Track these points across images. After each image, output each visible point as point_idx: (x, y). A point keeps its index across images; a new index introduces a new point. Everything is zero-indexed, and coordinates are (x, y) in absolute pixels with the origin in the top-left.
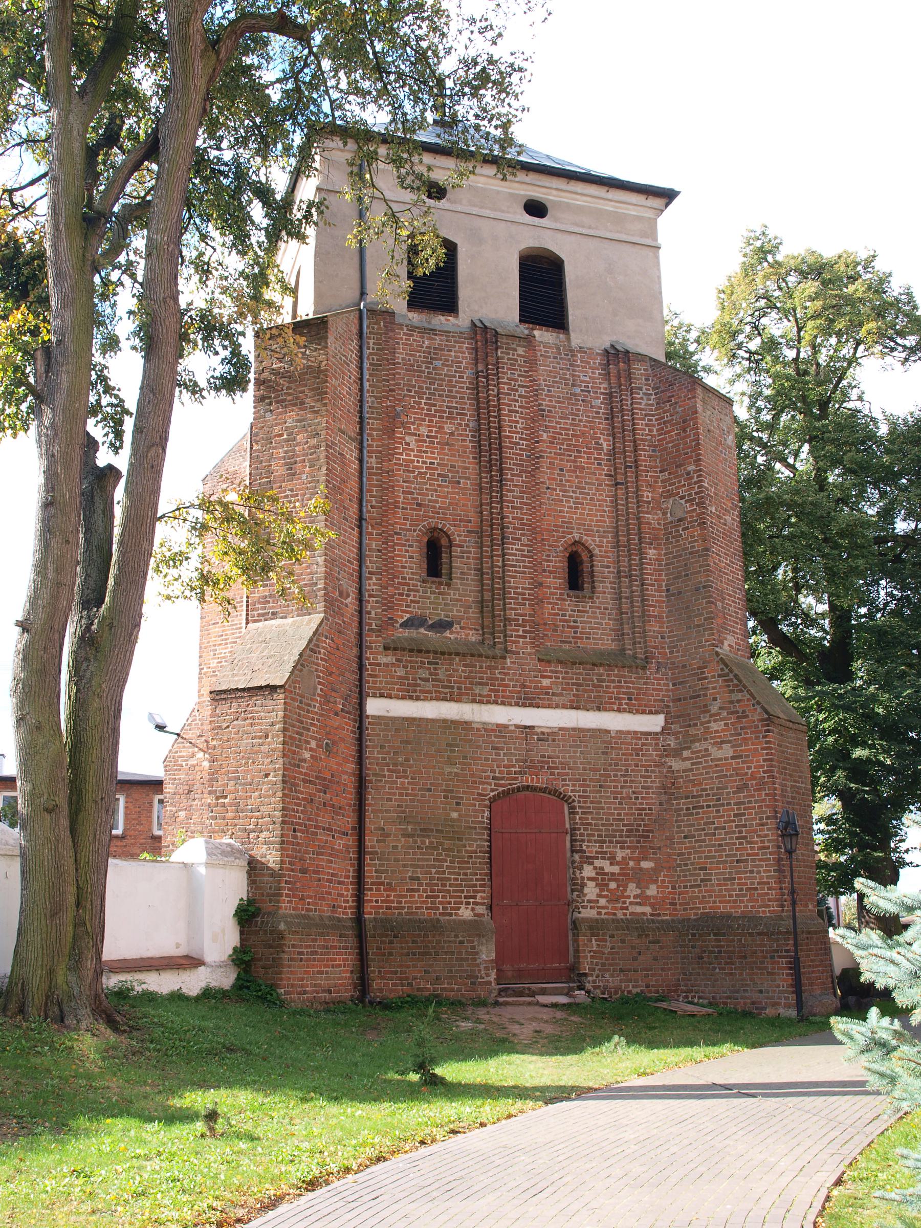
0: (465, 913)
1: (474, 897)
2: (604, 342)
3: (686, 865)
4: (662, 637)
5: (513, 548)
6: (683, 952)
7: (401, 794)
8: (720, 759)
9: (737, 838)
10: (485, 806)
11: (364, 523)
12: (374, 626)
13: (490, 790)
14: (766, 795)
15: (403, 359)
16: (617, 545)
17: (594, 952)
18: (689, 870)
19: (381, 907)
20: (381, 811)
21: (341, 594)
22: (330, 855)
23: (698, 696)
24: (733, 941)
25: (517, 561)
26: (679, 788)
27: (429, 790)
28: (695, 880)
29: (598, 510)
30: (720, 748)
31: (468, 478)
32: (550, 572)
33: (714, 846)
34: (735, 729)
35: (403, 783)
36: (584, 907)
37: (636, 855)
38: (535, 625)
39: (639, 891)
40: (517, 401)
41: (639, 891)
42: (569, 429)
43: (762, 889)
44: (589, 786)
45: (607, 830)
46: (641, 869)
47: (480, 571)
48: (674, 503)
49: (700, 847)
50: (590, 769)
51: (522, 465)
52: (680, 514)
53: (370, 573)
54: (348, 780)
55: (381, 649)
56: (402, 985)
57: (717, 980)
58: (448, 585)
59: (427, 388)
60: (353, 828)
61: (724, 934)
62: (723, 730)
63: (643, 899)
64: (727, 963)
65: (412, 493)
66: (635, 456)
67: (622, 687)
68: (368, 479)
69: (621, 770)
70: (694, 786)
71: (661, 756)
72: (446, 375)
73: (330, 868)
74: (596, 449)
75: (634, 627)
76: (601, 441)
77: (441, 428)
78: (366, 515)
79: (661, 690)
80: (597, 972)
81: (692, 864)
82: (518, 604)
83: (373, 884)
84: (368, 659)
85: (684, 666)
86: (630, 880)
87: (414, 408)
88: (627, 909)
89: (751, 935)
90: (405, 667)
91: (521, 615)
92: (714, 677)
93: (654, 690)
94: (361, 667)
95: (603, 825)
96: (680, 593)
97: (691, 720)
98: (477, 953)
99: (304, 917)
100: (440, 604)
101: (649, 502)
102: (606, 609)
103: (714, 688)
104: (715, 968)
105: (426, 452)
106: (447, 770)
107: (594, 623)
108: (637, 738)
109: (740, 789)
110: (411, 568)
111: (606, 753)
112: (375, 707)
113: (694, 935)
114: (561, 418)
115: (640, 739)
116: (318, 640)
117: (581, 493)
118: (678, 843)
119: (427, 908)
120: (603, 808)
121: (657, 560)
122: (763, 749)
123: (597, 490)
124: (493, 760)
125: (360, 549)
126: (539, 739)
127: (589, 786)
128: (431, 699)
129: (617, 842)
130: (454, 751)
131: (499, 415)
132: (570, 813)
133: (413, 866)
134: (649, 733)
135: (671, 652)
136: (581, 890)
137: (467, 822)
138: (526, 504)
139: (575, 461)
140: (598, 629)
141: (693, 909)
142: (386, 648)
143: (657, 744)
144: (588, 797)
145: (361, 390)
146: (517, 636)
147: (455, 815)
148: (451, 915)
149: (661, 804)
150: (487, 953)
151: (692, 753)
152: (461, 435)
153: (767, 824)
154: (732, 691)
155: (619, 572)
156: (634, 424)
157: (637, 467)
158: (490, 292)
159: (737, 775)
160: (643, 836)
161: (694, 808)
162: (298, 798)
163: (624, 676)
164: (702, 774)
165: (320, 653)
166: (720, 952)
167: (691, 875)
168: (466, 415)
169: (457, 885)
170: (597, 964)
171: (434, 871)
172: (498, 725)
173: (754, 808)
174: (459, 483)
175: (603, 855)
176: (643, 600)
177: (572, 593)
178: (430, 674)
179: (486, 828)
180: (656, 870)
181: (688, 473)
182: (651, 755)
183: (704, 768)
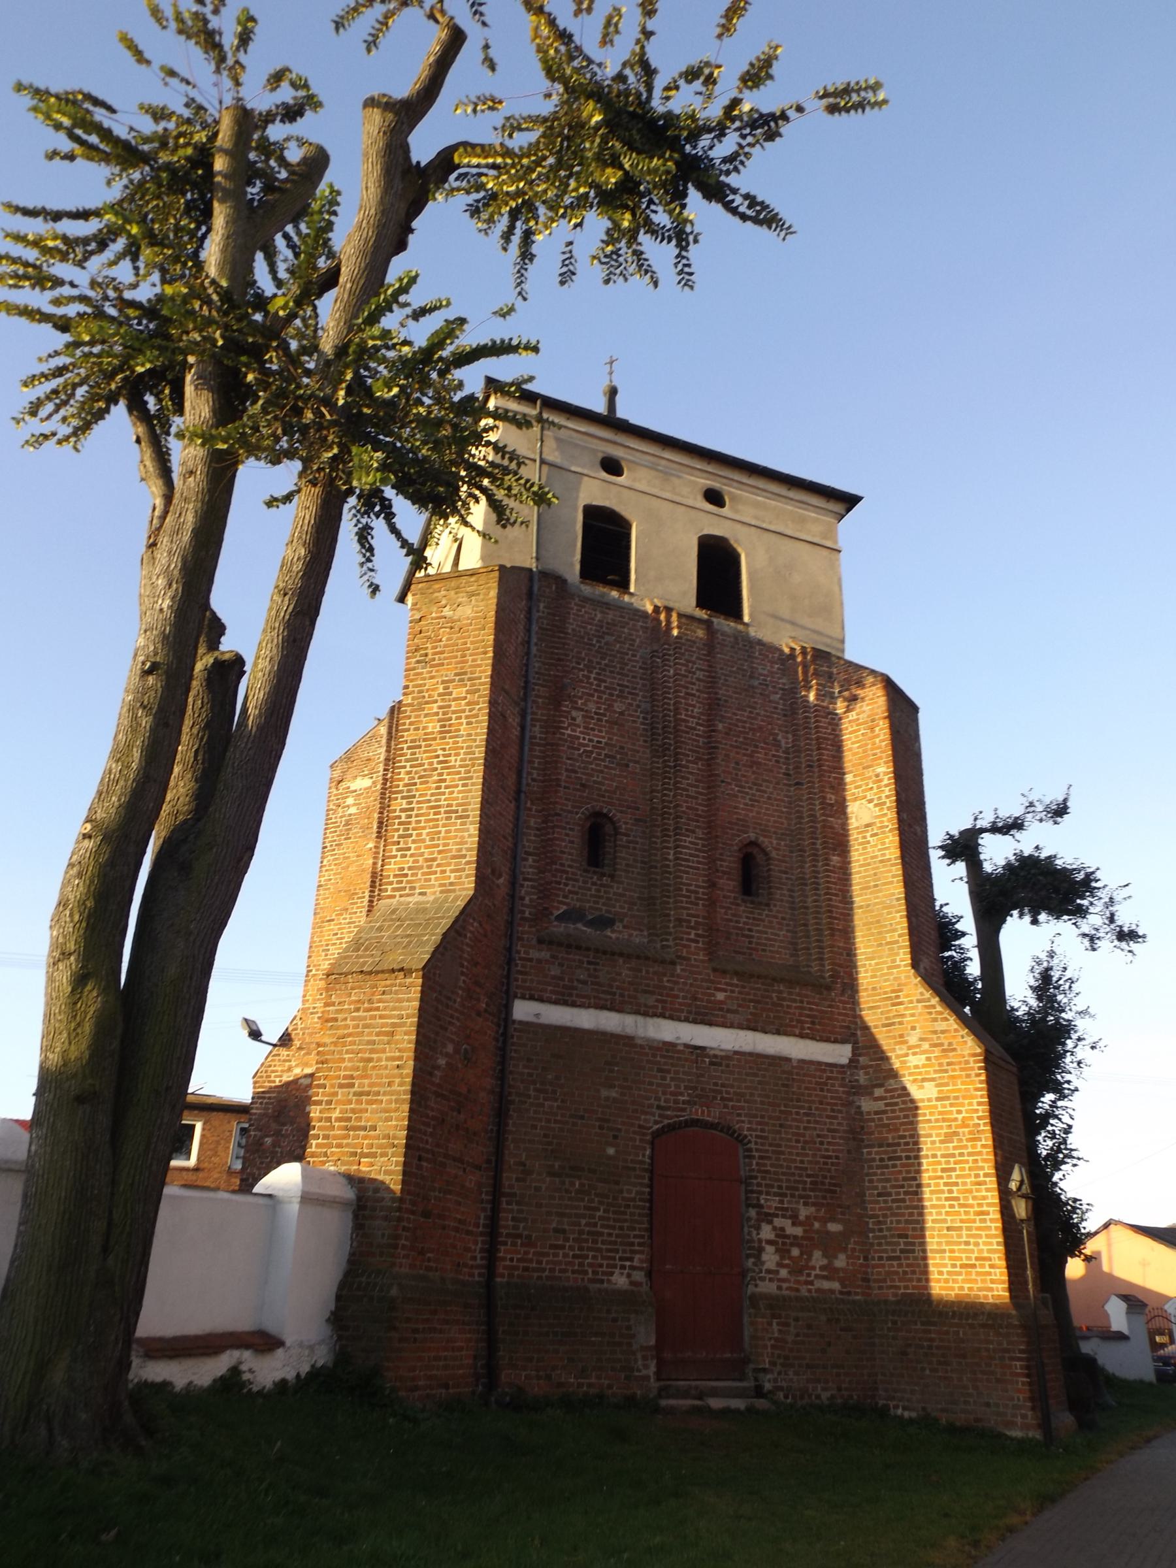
0: (620, 1281)
1: (631, 1259)
7: (548, 1121)
9: (947, 1199)
11: (523, 796)
12: (527, 915)
15: (573, 630)
17: (776, 1339)
18: (885, 1237)
19: (517, 1268)
21: (493, 872)
23: (893, 1024)
24: (947, 1333)
25: (691, 855)
27: (582, 1118)
28: (894, 1251)
29: (776, 811)
30: (922, 1087)
32: (724, 873)
34: (940, 1065)
36: (762, 1279)
37: (822, 1213)
39: (825, 1262)
40: (694, 684)
41: (825, 1262)
42: (745, 722)
43: (983, 1266)
44: (767, 1124)
45: (788, 1181)
46: (828, 1232)
49: (899, 1208)
51: (698, 752)
52: (867, 819)
53: (527, 853)
55: (534, 942)
58: (612, 876)
60: (489, 1161)
61: (934, 1324)
62: (924, 1066)
63: (830, 1272)
65: (576, 772)
68: (531, 750)
69: (802, 1107)
70: (890, 1131)
71: (848, 1093)
72: (618, 652)
74: (774, 745)
76: (779, 738)
77: (611, 706)
78: (524, 788)
80: (779, 1368)
81: (889, 1229)
82: (691, 903)
83: (508, 1235)
85: (874, 989)
87: (582, 681)
88: (811, 1283)
89: (972, 1326)
90: (561, 965)
91: (694, 916)
92: (911, 1002)
93: (840, 1014)
94: (510, 961)
95: (783, 1174)
98: (634, 1336)
100: (601, 897)
101: (831, 805)
102: (783, 919)
103: (912, 1015)
104: (923, 1369)
105: (593, 729)
106: (604, 1093)
109: (948, 1138)
110: (570, 854)
113: (894, 1323)
116: (464, 921)
117: (758, 790)
119: (573, 1272)
120: (783, 1153)
123: (775, 788)
124: (659, 1085)
125: (516, 826)
126: (712, 1063)
127: (767, 1124)
128: (589, 1007)
129: (801, 1197)
130: (612, 1071)
138: (701, 794)
139: (752, 756)
140: (775, 940)
142: (540, 941)
143: (843, 1079)
144: (766, 1138)
145: (528, 654)
146: (688, 940)
147: (611, 1151)
148: (602, 1281)
149: (849, 1152)
151: (887, 1091)
152: (632, 716)
153: (985, 1183)
154: (935, 1020)
159: (944, 1120)
161: (890, 1159)
162: (427, 1116)
163: (807, 996)
164: (898, 1118)
165: (465, 936)
166: (930, 1347)
167: (888, 1244)
169: (610, 1243)
170: (779, 1357)
171: (583, 1222)
172: (665, 1043)
173: (967, 1162)
174: (627, 766)
175: (783, 1212)
177: (746, 898)
178: (589, 976)
179: (645, 1170)
181: (877, 776)
182: (837, 1092)
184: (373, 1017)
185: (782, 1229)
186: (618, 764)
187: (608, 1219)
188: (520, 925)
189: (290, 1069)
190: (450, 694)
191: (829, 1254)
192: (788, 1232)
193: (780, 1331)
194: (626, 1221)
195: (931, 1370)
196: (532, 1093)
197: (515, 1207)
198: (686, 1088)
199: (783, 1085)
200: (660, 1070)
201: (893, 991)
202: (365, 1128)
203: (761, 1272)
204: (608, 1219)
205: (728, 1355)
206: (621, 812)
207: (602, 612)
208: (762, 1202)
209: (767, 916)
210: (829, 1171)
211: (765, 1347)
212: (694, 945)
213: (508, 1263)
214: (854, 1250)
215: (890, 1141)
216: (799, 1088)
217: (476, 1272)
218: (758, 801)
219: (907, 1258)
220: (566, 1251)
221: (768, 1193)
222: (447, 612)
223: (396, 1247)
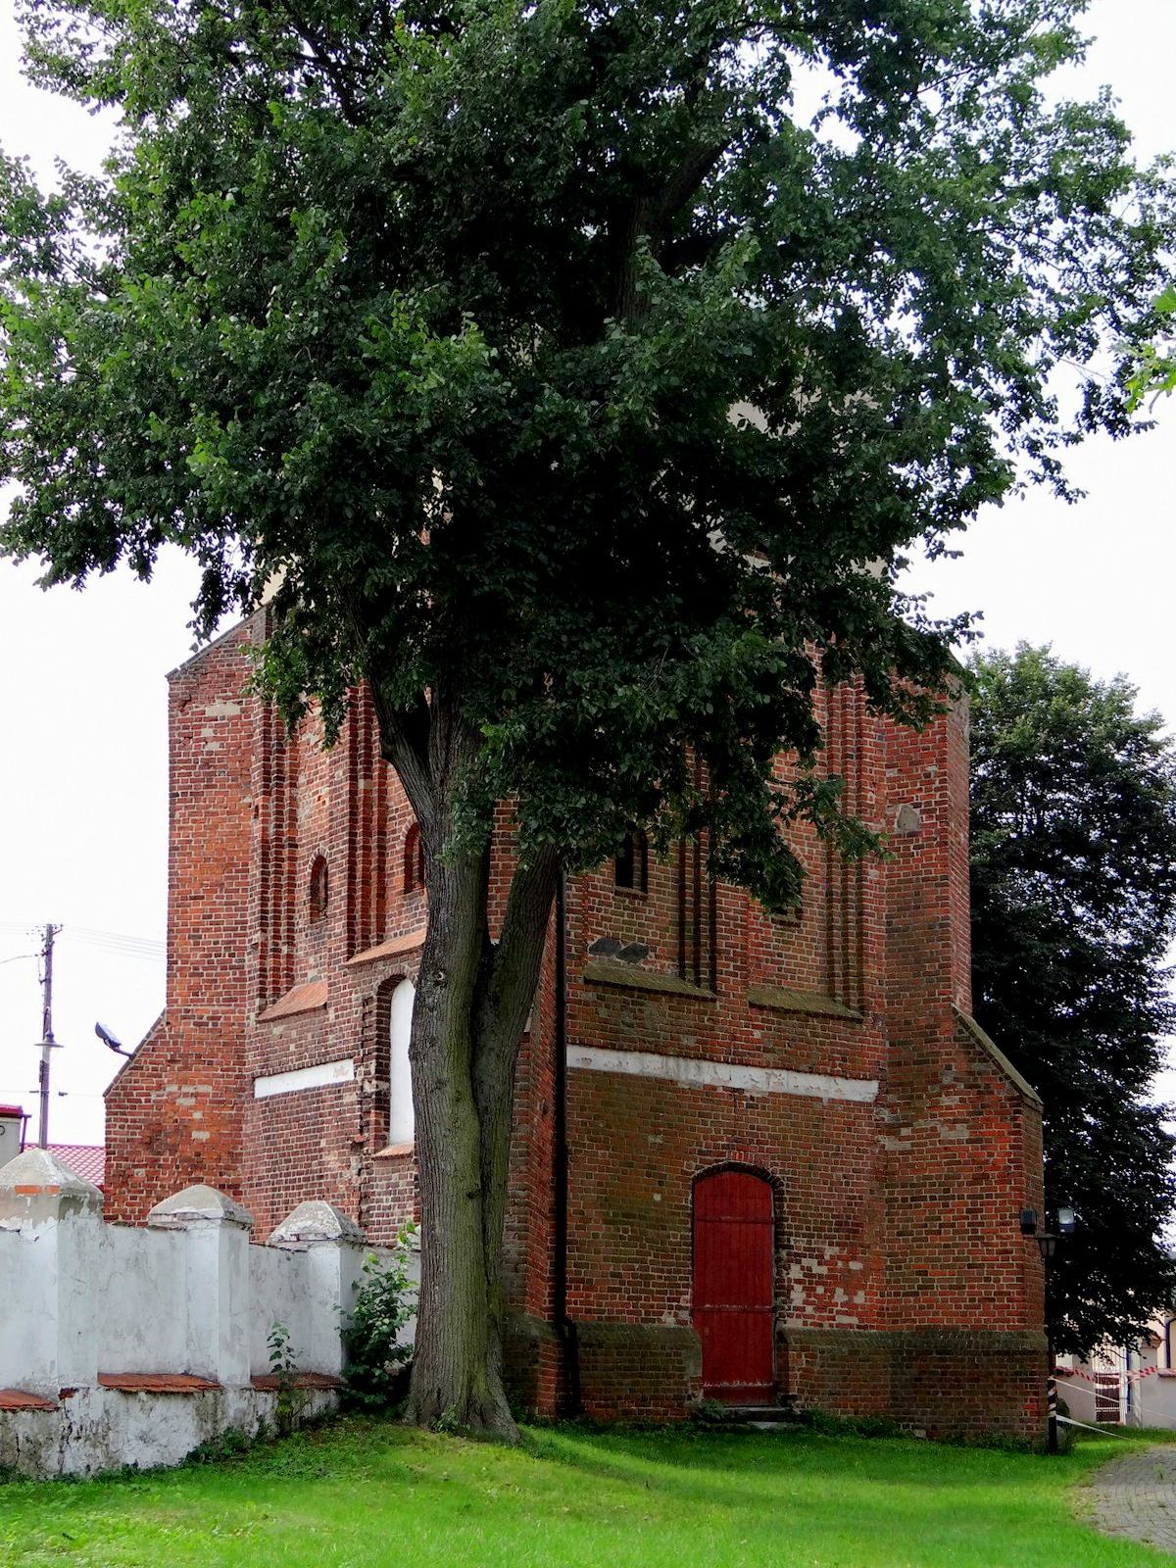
0: (669, 1320)
6: (895, 1373)
8: (952, 1142)
14: (1012, 1189)
30: (951, 1129)
39: (846, 1298)
41: (846, 1298)
46: (849, 1271)
52: (912, 826)
55: (581, 981)
56: (606, 1406)
58: (644, 899)
63: (850, 1308)
75: (848, 967)
79: (876, 1050)
82: (730, 931)
86: (837, 1284)
93: (870, 1049)
95: (812, 1215)
97: (913, 1090)
106: (651, 1139)
109: (976, 1180)
112: (575, 1056)
118: (889, 1241)
120: (812, 1195)
121: (878, 883)
129: (826, 1237)
133: (614, 1260)
137: (670, 1207)
141: (905, 1321)
146: (727, 973)
147: (657, 1197)
148: (653, 1321)
149: (872, 1192)
150: (694, 1369)
161: (913, 1199)
169: (660, 1285)
171: (637, 1266)
172: (705, 1086)
180: (864, 1273)
181: (928, 775)
189: (160, 1087)
191: (850, 1292)
214: (872, 1287)
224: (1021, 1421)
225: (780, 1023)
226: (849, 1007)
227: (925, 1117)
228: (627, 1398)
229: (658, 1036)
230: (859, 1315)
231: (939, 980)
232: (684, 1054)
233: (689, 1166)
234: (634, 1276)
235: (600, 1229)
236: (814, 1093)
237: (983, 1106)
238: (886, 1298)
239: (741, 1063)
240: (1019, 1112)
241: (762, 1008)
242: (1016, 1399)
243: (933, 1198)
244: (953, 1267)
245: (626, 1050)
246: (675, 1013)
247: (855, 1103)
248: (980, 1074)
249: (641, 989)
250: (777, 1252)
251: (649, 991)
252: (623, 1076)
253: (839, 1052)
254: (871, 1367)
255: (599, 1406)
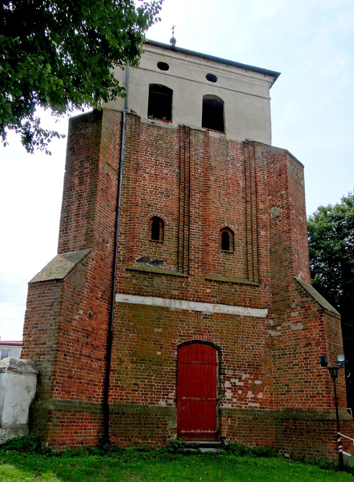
0: (162, 403)
2: (241, 139)
3: (278, 383)
4: (267, 272)
5: (193, 226)
6: (276, 428)
8: (297, 331)
9: (305, 370)
10: (175, 349)
11: (119, 209)
13: (178, 342)
14: (321, 348)
16: (246, 230)
18: (280, 386)
20: (120, 350)
21: (103, 241)
22: (89, 370)
25: (196, 232)
26: (275, 345)
27: (146, 340)
31: (174, 195)
32: (213, 240)
33: (293, 374)
34: (305, 316)
35: (133, 336)
36: (225, 402)
37: (252, 377)
38: (204, 263)
39: (253, 396)
41: (253, 396)
42: (224, 176)
43: (319, 397)
46: (255, 384)
47: (178, 238)
48: (274, 210)
49: (286, 374)
50: (230, 334)
52: (277, 214)
53: (121, 233)
54: (103, 333)
55: (125, 270)
56: (126, 440)
57: (294, 444)
58: (162, 243)
59: (155, 153)
62: (298, 316)
63: (255, 400)
64: (299, 435)
66: (256, 188)
67: (247, 295)
69: (245, 335)
72: (165, 148)
73: (89, 377)
74: (237, 186)
75: (254, 267)
76: (240, 182)
78: (119, 206)
79: (266, 297)
80: (231, 436)
81: (281, 383)
82: (196, 252)
83: (113, 386)
84: (117, 274)
88: (247, 404)
90: (137, 279)
91: (197, 258)
96: (276, 251)
97: (281, 311)
98: (167, 424)
99: (67, 402)
100: (157, 252)
101: (262, 210)
104: (293, 437)
106: (156, 330)
107: (234, 266)
108: (254, 320)
111: (238, 326)
112: (119, 298)
114: (220, 171)
115: (255, 320)
118: (274, 372)
120: (235, 353)
122: (319, 325)
123: (237, 204)
124: (180, 327)
126: (204, 318)
127: (229, 342)
128: (149, 296)
129: (243, 370)
130: (160, 322)
131: (190, 165)
132: (219, 355)
134: (260, 318)
135: (271, 280)
136: (224, 394)
140: (236, 268)
141: (281, 405)
143: (264, 323)
147: (159, 353)
148: (154, 404)
149: (265, 352)
150: (172, 424)
151: (282, 327)
154: (303, 297)
155: (247, 242)
156: (256, 174)
157: (256, 193)
158: (187, 112)
159: (305, 338)
160: (255, 368)
161: (282, 355)
167: (281, 388)
168: (174, 166)
169: (158, 389)
171: (146, 381)
172: (183, 310)
174: (169, 196)
175: (235, 376)
176: (258, 255)
178: (149, 283)
180: (263, 385)
181: (282, 195)
182: (261, 328)
183: (288, 335)
184: (45, 300)
185: (235, 383)
186: (165, 196)
187: (158, 380)
188: (118, 263)
190: (84, 166)
191: (255, 392)
192: (237, 384)
193: (231, 422)
194: (165, 380)
195: (296, 438)
196: (124, 330)
197: (116, 375)
198: (192, 328)
199: (236, 326)
200: (180, 321)
201: (286, 286)
202: (42, 344)
203: (225, 399)
204: (158, 380)
205: (210, 431)
206: (166, 216)
207: (158, 131)
208: (226, 372)
209: (232, 258)
210: (256, 360)
211: (225, 428)
212: (196, 270)
213: (114, 397)
214: (266, 391)
215: (283, 348)
216: (244, 327)
217: (100, 400)
218: (229, 210)
219: (288, 394)
220: (139, 392)
221: (228, 369)
222: (83, 131)
223: (53, 390)
224: (329, 453)
225: (219, 287)
226: (254, 282)
227: (286, 322)
228: (137, 437)
229: (160, 291)
230: (260, 403)
231: (289, 268)
232: (172, 297)
233: (175, 341)
234: (145, 385)
235: (129, 365)
236: (237, 314)
237: (308, 315)
238: (273, 396)
239: (200, 301)
240: (322, 316)
241: (210, 281)
242: (326, 442)
243: (290, 354)
244: (298, 382)
245: (145, 296)
246: (169, 282)
247: (256, 317)
248: (305, 302)
249: (152, 273)
250: (219, 376)
251: (156, 274)
252: (144, 305)
253: (248, 298)
254: (265, 425)
255: (122, 440)
